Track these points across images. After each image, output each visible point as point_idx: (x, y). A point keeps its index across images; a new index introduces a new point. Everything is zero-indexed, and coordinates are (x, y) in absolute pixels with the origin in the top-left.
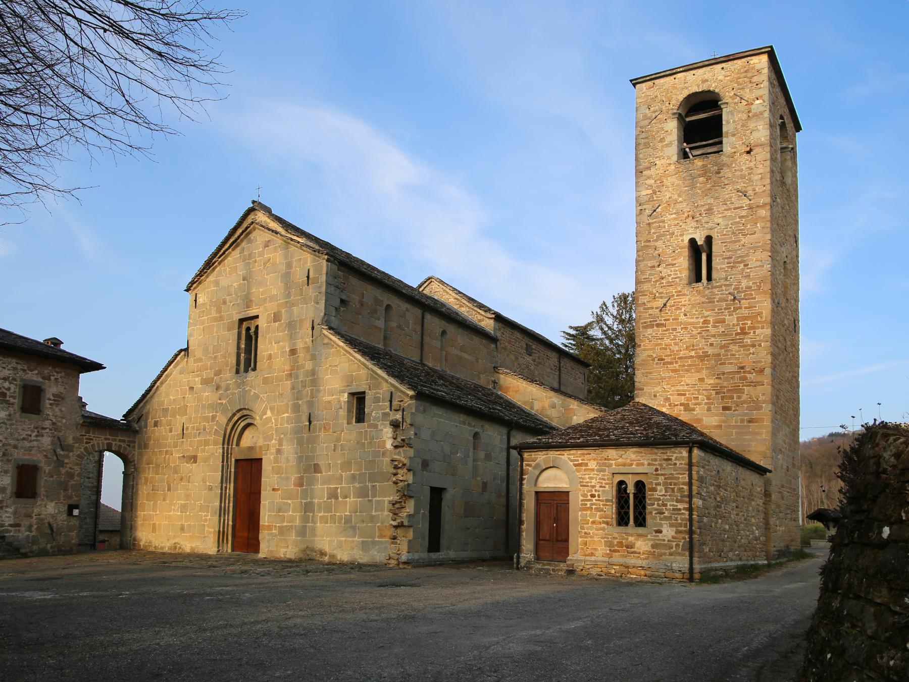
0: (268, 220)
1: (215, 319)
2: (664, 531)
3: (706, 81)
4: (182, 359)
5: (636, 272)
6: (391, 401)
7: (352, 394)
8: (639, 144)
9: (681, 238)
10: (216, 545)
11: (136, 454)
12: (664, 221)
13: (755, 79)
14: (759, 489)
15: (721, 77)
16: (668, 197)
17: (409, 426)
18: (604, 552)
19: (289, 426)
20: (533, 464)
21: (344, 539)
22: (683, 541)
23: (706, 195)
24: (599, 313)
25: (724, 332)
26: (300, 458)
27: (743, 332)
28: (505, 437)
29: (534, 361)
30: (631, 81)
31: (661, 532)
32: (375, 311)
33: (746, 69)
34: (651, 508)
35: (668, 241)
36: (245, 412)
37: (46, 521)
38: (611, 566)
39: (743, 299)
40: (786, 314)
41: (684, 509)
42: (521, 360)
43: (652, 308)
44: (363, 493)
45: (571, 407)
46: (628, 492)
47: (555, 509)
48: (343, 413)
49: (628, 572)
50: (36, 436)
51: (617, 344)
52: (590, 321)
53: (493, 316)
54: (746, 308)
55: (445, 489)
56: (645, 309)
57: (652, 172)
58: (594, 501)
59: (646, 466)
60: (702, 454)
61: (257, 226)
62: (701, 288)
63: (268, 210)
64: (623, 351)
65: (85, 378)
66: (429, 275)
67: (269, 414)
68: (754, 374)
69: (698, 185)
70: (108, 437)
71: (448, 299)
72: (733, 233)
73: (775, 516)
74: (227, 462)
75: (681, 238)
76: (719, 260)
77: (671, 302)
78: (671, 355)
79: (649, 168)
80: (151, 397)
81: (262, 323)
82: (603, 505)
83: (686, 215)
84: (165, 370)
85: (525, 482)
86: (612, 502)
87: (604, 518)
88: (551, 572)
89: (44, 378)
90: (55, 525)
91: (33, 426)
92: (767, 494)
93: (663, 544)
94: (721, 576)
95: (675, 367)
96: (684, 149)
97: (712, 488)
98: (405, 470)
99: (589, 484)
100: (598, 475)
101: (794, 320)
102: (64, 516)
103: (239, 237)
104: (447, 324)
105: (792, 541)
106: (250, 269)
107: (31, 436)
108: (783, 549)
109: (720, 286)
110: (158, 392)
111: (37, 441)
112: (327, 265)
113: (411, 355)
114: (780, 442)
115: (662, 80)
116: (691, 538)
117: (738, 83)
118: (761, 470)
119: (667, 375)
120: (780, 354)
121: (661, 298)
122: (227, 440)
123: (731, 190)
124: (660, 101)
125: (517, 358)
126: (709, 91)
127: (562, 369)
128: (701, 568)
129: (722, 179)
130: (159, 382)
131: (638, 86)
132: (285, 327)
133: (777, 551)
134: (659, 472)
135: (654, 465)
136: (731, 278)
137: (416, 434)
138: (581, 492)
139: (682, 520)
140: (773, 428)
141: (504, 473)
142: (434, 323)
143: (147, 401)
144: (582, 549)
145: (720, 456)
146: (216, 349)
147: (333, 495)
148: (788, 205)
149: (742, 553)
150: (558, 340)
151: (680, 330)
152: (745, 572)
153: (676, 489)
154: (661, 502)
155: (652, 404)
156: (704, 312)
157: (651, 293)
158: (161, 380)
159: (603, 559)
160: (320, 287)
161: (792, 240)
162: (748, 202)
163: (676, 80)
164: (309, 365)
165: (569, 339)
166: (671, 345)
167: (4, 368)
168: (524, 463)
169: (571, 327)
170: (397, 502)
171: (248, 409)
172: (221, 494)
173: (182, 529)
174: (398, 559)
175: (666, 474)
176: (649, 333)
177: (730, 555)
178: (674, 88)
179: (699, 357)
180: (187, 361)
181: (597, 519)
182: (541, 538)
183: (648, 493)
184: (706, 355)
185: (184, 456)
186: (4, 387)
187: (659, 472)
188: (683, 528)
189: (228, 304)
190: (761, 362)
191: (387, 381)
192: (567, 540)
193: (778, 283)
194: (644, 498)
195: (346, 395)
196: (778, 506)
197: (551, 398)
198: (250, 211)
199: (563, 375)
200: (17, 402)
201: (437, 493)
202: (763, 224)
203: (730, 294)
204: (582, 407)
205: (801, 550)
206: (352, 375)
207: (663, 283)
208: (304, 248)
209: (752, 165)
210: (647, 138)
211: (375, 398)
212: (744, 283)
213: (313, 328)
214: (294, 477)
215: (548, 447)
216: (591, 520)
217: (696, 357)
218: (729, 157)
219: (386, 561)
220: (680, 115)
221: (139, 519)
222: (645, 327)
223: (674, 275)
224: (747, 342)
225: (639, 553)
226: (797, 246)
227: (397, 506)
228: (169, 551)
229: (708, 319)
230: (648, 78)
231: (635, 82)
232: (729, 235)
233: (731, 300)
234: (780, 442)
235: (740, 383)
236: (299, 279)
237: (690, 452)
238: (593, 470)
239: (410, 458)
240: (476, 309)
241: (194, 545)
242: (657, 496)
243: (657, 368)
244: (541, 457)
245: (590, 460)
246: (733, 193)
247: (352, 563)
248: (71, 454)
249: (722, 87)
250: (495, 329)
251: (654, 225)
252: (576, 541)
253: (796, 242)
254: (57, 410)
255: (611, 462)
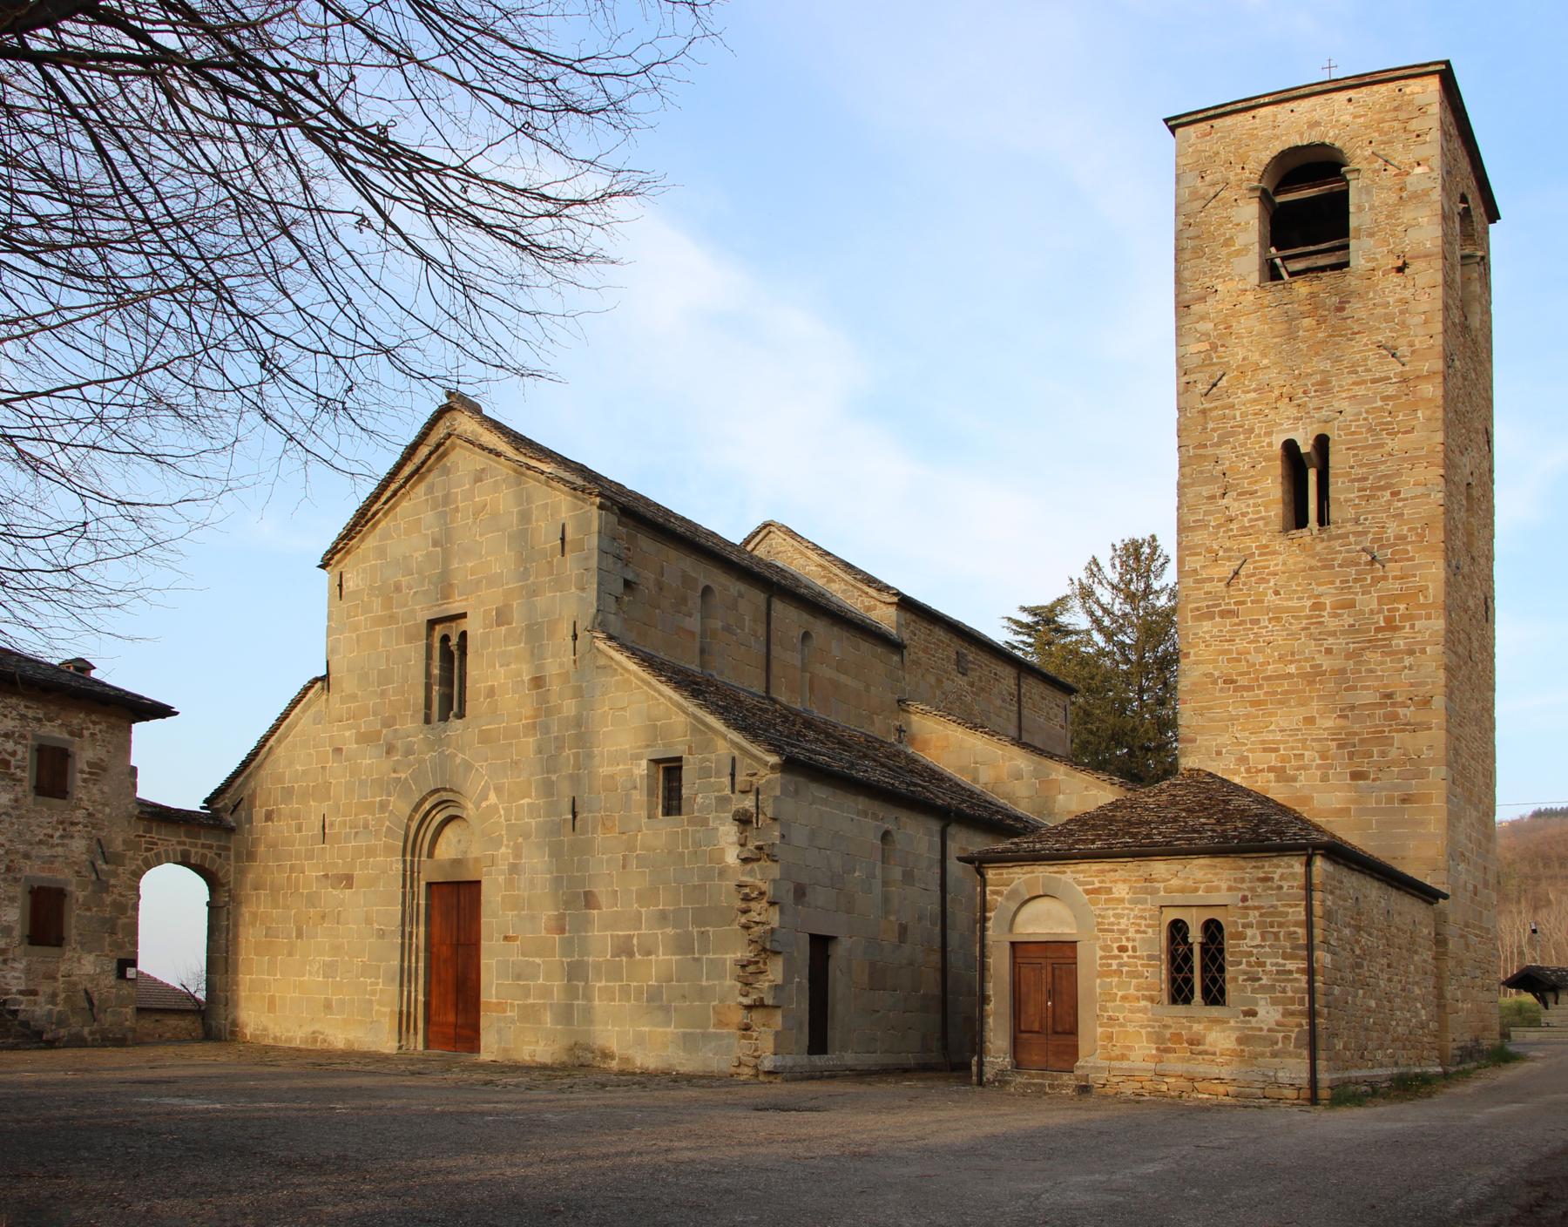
0: (480, 430)
1: (379, 621)
2: (1262, 1012)
3: (1317, 124)
4: (318, 696)
5: (1178, 508)
6: (733, 775)
7: (657, 762)
8: (1183, 249)
9: (1267, 440)
10: (397, 1038)
11: (232, 869)
12: (1232, 407)
13: (1414, 125)
14: (1425, 931)
15: (1347, 118)
16: (1240, 357)
17: (769, 821)
18: (1147, 1052)
19: (533, 822)
20: (1006, 890)
21: (647, 1029)
22: (1296, 1030)
23: (1317, 354)
24: (1084, 581)
25: (1353, 625)
26: (557, 881)
27: (1391, 626)
28: (937, 839)
29: (972, 685)
30: (1166, 121)
31: (1253, 1014)
32: (684, 600)
33: (1396, 104)
34: (1234, 972)
35: (1241, 445)
36: (445, 796)
37: (80, 987)
38: (1160, 1078)
39: (1390, 560)
40: (1471, 587)
41: (1299, 970)
42: (947, 685)
43: (1211, 580)
44: (683, 945)
45: (1053, 776)
46: (1190, 940)
47: (1050, 975)
48: (639, 797)
49: (1194, 1089)
50: (62, 837)
51: (1123, 642)
52: (1060, 595)
53: (896, 599)
54: (1395, 578)
55: (833, 938)
56: (1197, 581)
57: (1210, 306)
58: (1126, 959)
59: (1224, 892)
60: (1329, 867)
61: (458, 441)
62: (1308, 539)
63: (476, 410)
64: (1134, 658)
65: (143, 733)
66: (767, 519)
67: (492, 798)
68: (1412, 708)
69: (1301, 333)
70: (183, 839)
71: (804, 567)
72: (1370, 430)
73: (1453, 982)
74: (412, 886)
75: (1267, 440)
76: (1343, 483)
77: (1248, 568)
78: (1249, 673)
79: (1202, 299)
80: (260, 766)
81: (472, 626)
82: (1142, 965)
83: (1277, 393)
84: (284, 716)
85: (989, 924)
86: (1160, 960)
87: (1146, 989)
88: (1047, 1089)
89: (72, 734)
90: (96, 995)
91: (55, 819)
92: (1440, 941)
93: (1260, 1037)
94: (1365, 1094)
95: (1257, 695)
96: (1272, 259)
97: (1347, 931)
98: (764, 903)
99: (1115, 927)
100: (1132, 909)
101: (1486, 599)
102: (111, 979)
103: (423, 463)
104: (811, 619)
105: (1485, 1029)
106: (445, 523)
107: (52, 837)
108: (1469, 1044)
109: (1346, 536)
110: (272, 758)
111: (63, 845)
112: (600, 516)
113: (749, 682)
114: (1462, 838)
115: (1229, 120)
116: (1312, 1025)
117: (1381, 132)
118: (1429, 895)
119: (1242, 711)
120: (1460, 667)
121: (1229, 559)
122: (411, 846)
123: (1366, 345)
124: (1225, 162)
125: (939, 681)
126: (1323, 144)
127: (1024, 699)
128: (1332, 1080)
129: (1349, 321)
130: (274, 738)
131: (1179, 131)
132: (521, 634)
133: (1458, 1048)
134: (1250, 903)
135: (1240, 889)
136: (1366, 519)
137: (783, 836)
138: (1100, 943)
139: (1295, 991)
140: (1450, 813)
141: (937, 908)
142: (788, 617)
143: (250, 774)
144: (1104, 1047)
145: (1359, 871)
146: (385, 678)
147: (624, 949)
148: (1475, 370)
149: (1400, 1052)
150: (1000, 634)
151: (1267, 623)
152: (1407, 1087)
153: (1282, 934)
154: (1253, 959)
155: (1217, 767)
156: (1313, 586)
157: (1209, 550)
158: (277, 735)
159: (1144, 1065)
160: (587, 559)
161: (1482, 439)
162: (1400, 368)
163: (1257, 121)
164: (569, 707)
165: (1018, 633)
166: (1249, 653)
167: (5, 716)
168: (988, 889)
169: (1024, 609)
170: (750, 963)
171: (451, 790)
172: (403, 945)
173: (328, 1006)
174: (756, 1066)
175: (1262, 907)
176: (1205, 629)
177: (1379, 1054)
178: (1253, 136)
179: (1303, 676)
180: (327, 700)
181: (1132, 991)
182: (1023, 1028)
183: (1229, 943)
184: (1317, 672)
185: (326, 876)
186: (5, 750)
187: (1250, 903)
188: (1296, 1007)
189: (405, 591)
190: (1426, 684)
191: (724, 737)
192: (1073, 1032)
193: (1456, 527)
194: (1221, 951)
195: (644, 763)
196: (1460, 963)
197: (1012, 759)
198: (442, 412)
199: (1025, 712)
200: (27, 776)
201: (821, 945)
202: (1428, 413)
203: (1364, 550)
204: (1074, 777)
205: (1502, 1048)
206: (655, 726)
207: (1232, 530)
208: (554, 484)
209: (1407, 294)
210: (1199, 237)
211: (701, 768)
212: (1392, 529)
213: (575, 637)
214: (547, 914)
215: (1035, 858)
216: (1120, 994)
217: (1298, 675)
218: (1361, 277)
219: (733, 1070)
220: (1264, 191)
221: (241, 988)
222: (1196, 619)
223: (1253, 513)
224: (1398, 645)
225: (1214, 1054)
226: (1490, 450)
227: (751, 969)
228: (303, 1046)
229: (1322, 600)
230: (1200, 116)
231: (1173, 122)
232: (1361, 433)
233: (1366, 563)
234: (1462, 838)
235: (1384, 725)
236: (546, 543)
237: (1309, 864)
238: (1121, 900)
239: (774, 881)
240: (859, 585)
241: (351, 1037)
242: (1246, 948)
243: (1221, 698)
244: (1021, 877)
245: (1115, 882)
246: (1370, 350)
247: (666, 1073)
248: (121, 870)
249: (1348, 138)
250: (899, 625)
251: (1215, 413)
252: (1091, 1033)
253: (1489, 442)
254: (95, 790)
255: (1157, 885)
